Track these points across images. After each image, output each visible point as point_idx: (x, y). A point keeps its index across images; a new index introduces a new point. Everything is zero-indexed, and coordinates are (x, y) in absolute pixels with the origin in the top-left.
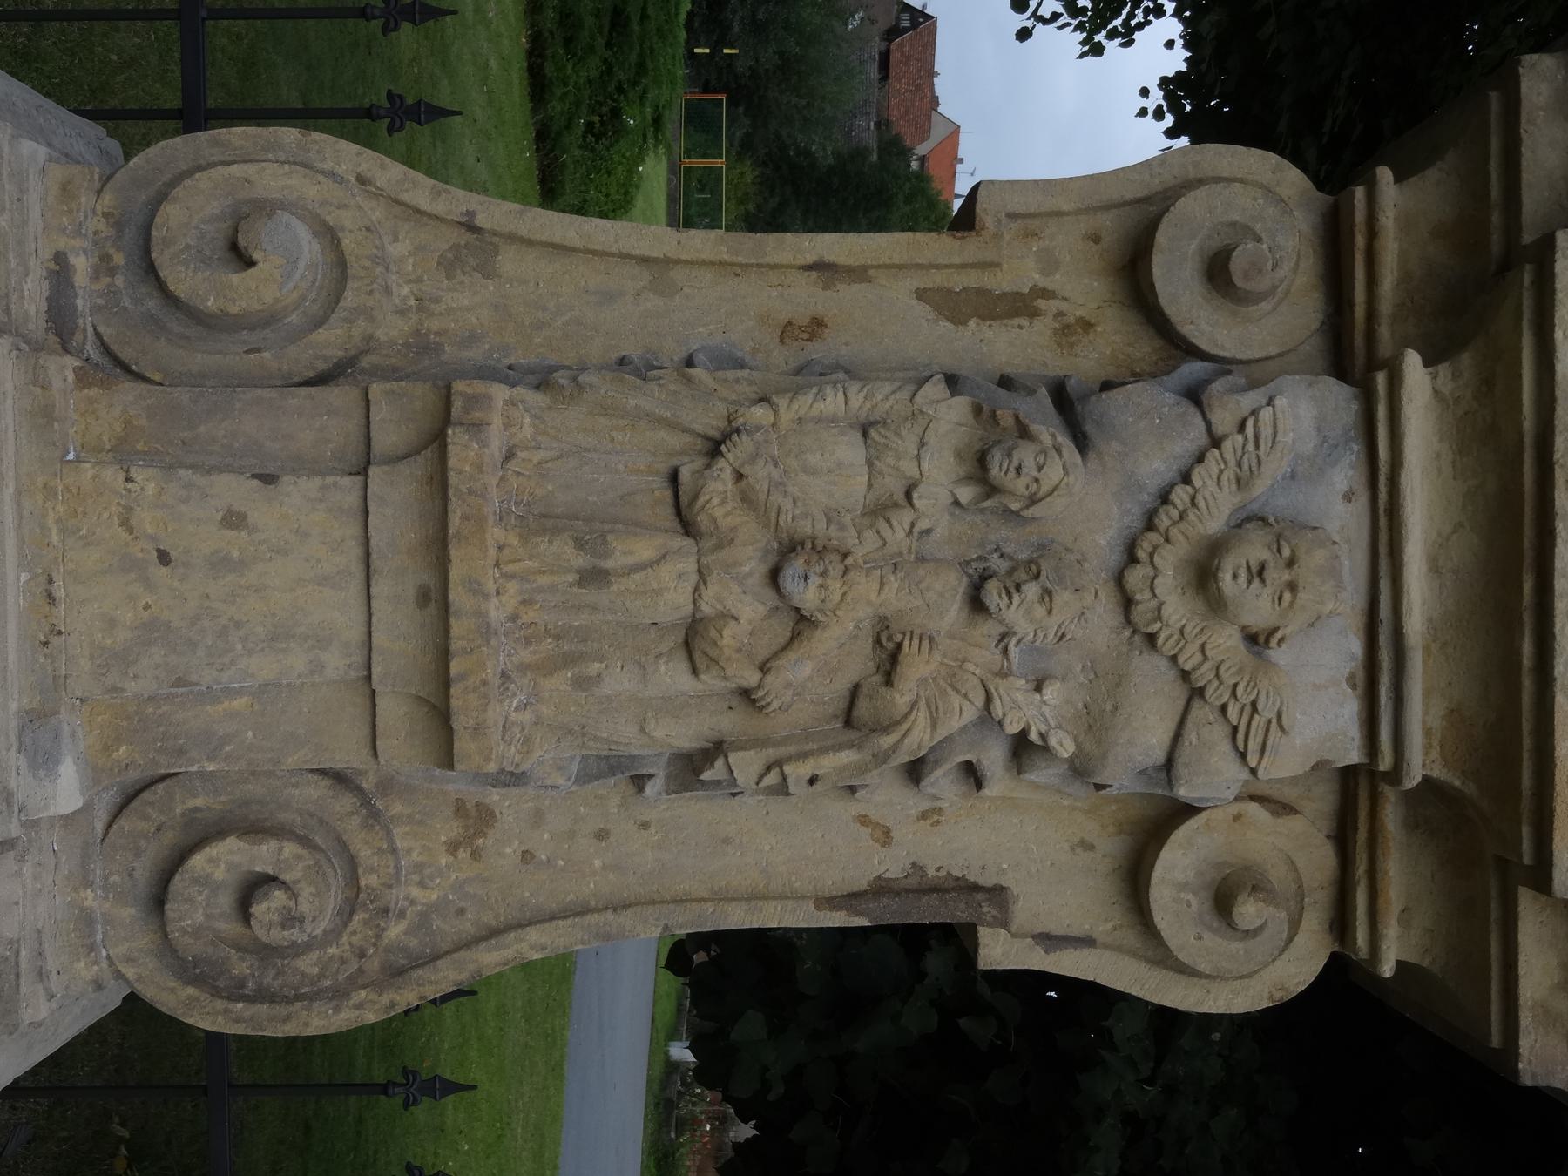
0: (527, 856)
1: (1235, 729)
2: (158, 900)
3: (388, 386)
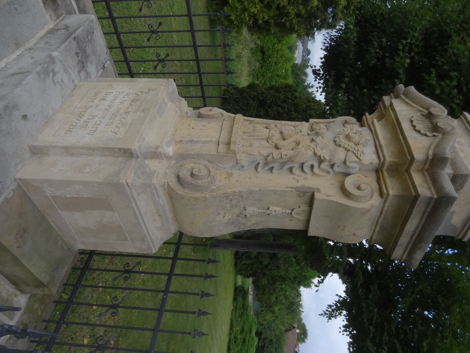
0: (237, 181)
1: (355, 154)
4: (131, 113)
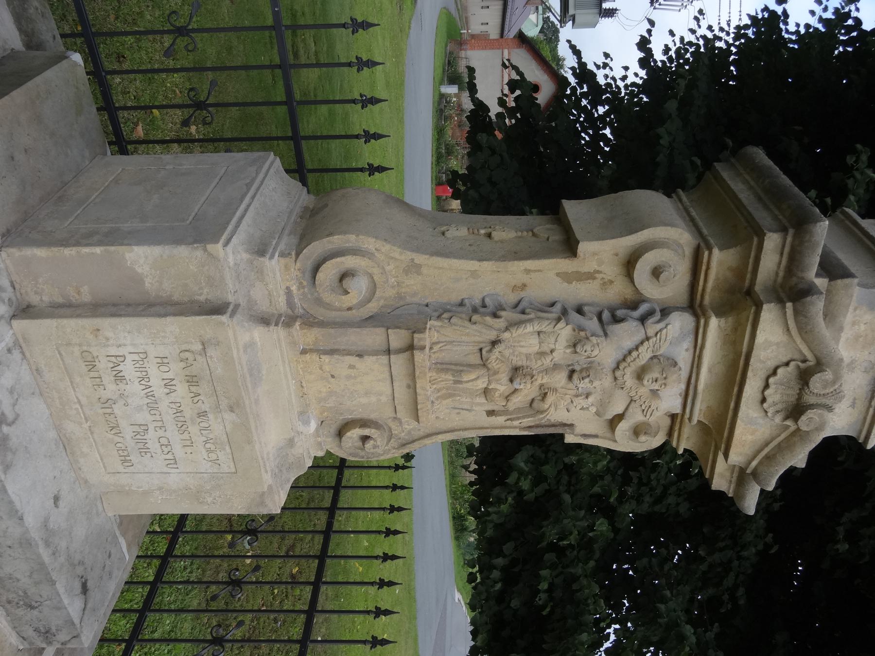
0: (437, 418)
3: (394, 330)
4: (211, 416)
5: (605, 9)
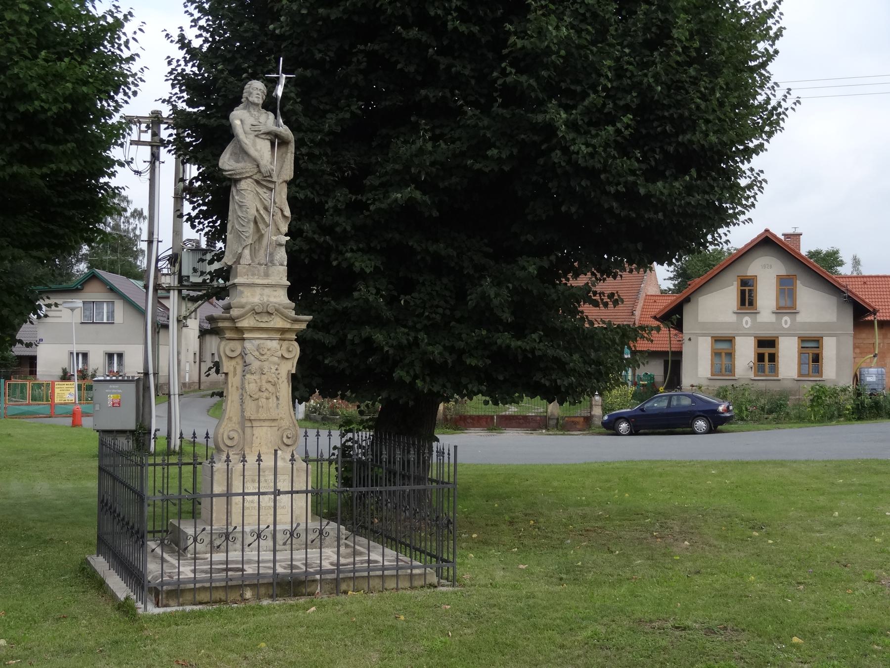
2: (288, 446)
5: (207, 245)
